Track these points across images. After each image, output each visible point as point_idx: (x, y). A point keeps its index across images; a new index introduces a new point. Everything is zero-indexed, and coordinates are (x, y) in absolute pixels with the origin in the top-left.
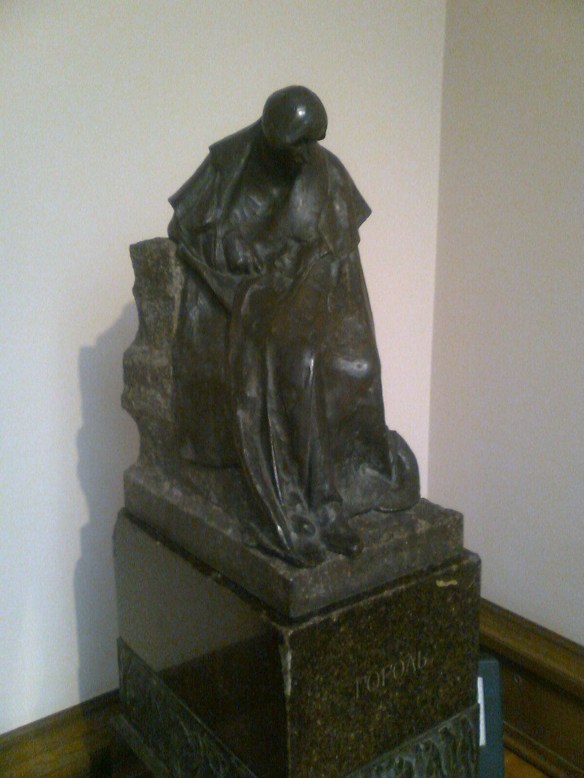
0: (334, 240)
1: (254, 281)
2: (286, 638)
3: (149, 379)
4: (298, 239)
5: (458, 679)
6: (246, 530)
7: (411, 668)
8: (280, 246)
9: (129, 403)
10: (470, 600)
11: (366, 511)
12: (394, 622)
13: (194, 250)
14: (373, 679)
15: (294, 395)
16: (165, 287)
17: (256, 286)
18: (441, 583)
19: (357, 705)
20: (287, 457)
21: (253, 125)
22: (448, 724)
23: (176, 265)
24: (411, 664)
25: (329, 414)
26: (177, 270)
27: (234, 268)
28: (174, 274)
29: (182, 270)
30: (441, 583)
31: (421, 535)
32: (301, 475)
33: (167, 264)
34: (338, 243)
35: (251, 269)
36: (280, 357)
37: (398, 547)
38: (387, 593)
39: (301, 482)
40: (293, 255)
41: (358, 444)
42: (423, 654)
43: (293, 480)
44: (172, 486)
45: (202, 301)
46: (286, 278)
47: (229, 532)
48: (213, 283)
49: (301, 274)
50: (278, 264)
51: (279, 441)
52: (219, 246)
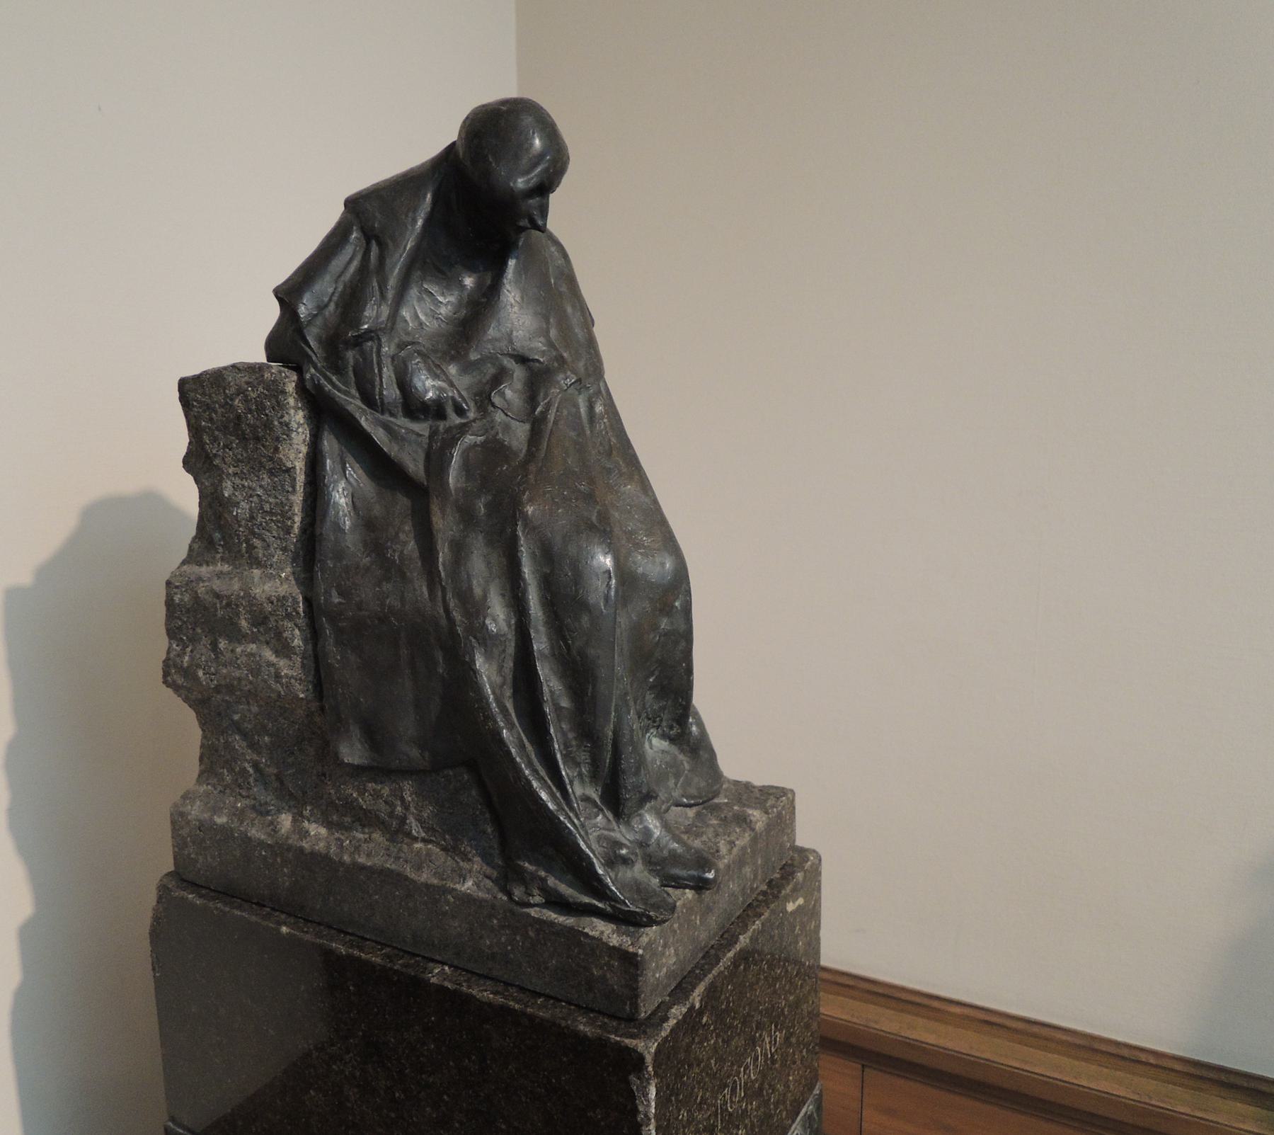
1: (463, 429)
2: (649, 1059)
3: (244, 623)
4: (522, 360)
6: (508, 876)
8: (491, 370)
9: (188, 673)
15: (585, 620)
16: (276, 450)
17: (469, 439)
20: (571, 735)
21: (444, 150)
24: (766, 1049)
26: (297, 417)
27: (414, 407)
28: (294, 425)
32: (595, 763)
33: (280, 406)
35: (450, 411)
36: (547, 555)
39: (594, 777)
40: (519, 385)
43: (580, 775)
44: (298, 818)
45: (355, 472)
46: (514, 424)
47: (468, 886)
48: (379, 436)
49: (544, 414)
50: (496, 400)
52: (388, 373)
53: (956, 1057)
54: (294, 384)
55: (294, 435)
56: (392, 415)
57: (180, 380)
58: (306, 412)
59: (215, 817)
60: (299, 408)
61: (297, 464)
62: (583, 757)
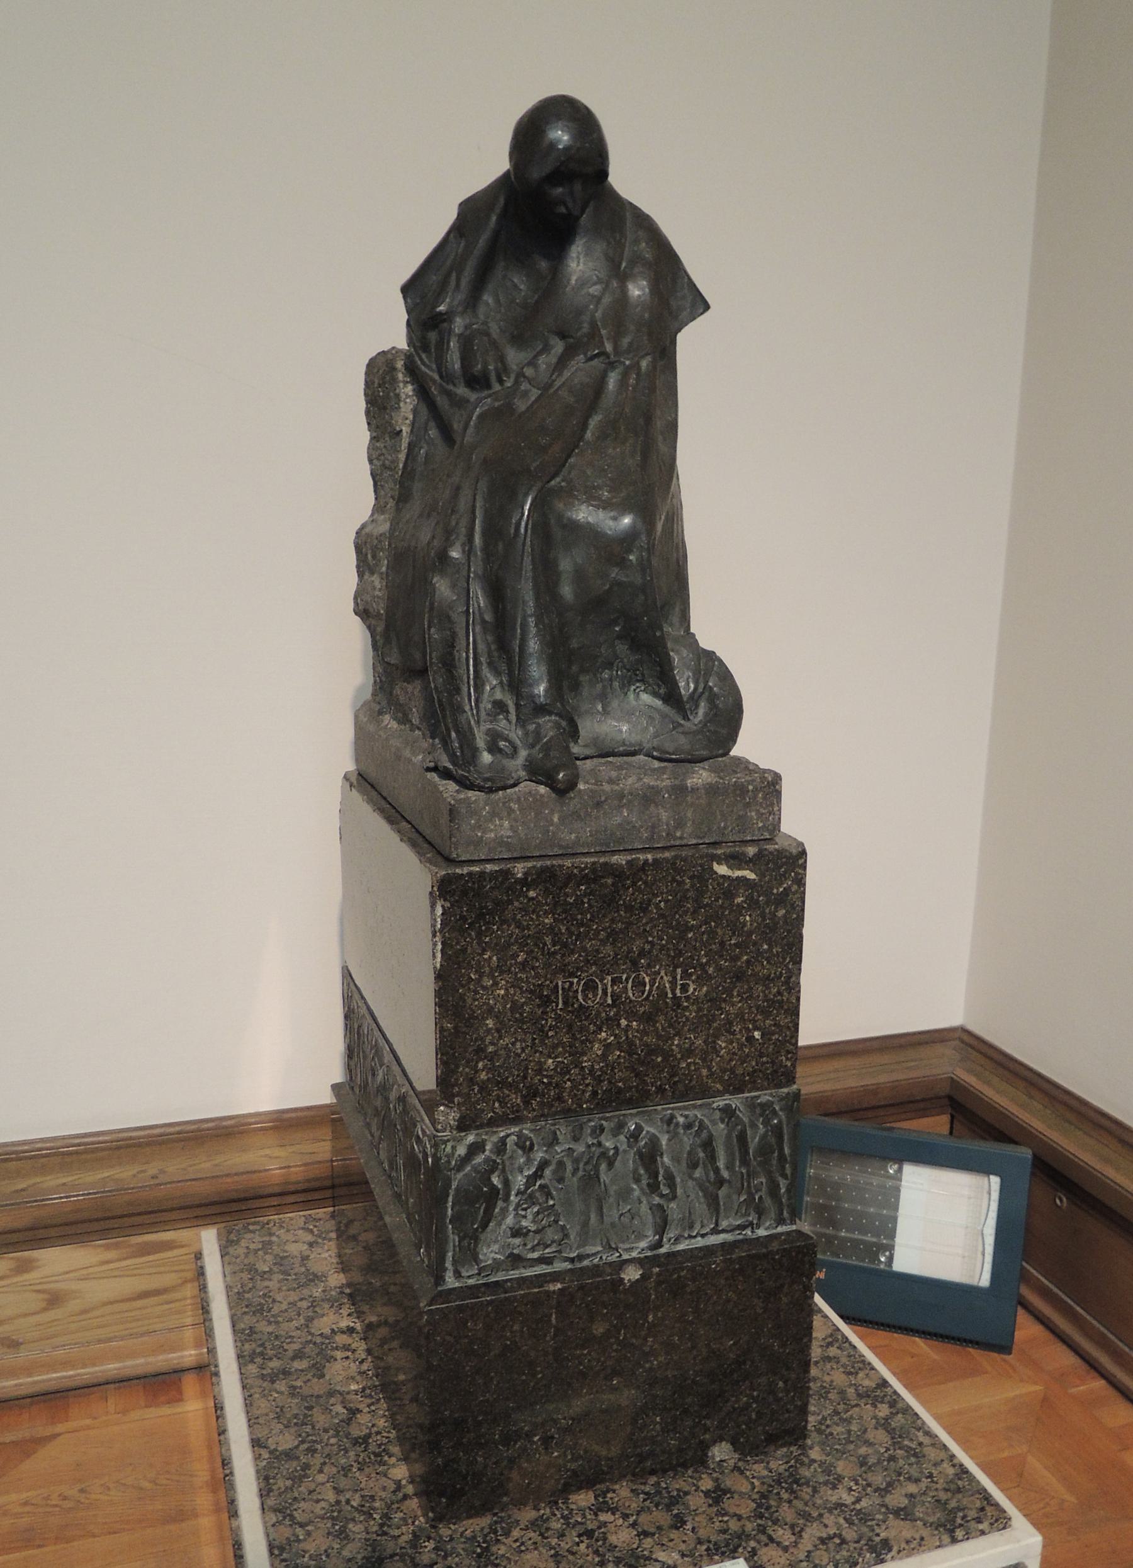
0: (616, 339)
5: (757, 1035)
7: (662, 994)
10: (781, 913)
11: (633, 754)
12: (629, 908)
13: (424, 356)
14: (590, 986)
18: (722, 869)
19: (558, 1018)
20: (493, 647)
22: (735, 1101)
23: (406, 383)
25: (567, 591)
28: (403, 396)
29: (414, 390)
30: (722, 869)
31: (694, 790)
32: (510, 674)
34: (625, 341)
37: (649, 798)
38: (619, 859)
41: (622, 648)
42: (686, 975)
43: (501, 683)
51: (483, 622)
53: (991, 1107)
54: (402, 362)
55: (402, 404)
56: (455, 385)
57: (371, 365)
58: (415, 386)
59: (715, 864)
60: (407, 382)
61: (404, 428)
62: (504, 667)
